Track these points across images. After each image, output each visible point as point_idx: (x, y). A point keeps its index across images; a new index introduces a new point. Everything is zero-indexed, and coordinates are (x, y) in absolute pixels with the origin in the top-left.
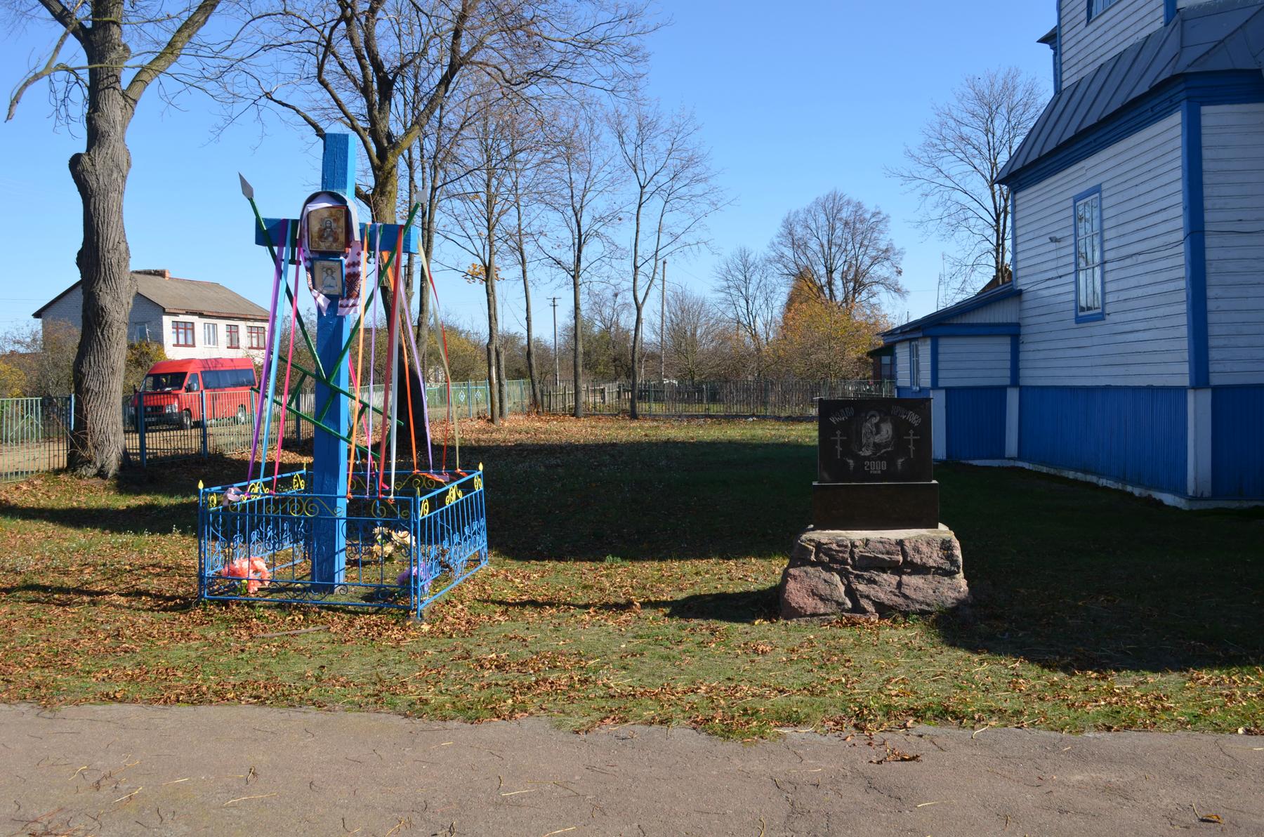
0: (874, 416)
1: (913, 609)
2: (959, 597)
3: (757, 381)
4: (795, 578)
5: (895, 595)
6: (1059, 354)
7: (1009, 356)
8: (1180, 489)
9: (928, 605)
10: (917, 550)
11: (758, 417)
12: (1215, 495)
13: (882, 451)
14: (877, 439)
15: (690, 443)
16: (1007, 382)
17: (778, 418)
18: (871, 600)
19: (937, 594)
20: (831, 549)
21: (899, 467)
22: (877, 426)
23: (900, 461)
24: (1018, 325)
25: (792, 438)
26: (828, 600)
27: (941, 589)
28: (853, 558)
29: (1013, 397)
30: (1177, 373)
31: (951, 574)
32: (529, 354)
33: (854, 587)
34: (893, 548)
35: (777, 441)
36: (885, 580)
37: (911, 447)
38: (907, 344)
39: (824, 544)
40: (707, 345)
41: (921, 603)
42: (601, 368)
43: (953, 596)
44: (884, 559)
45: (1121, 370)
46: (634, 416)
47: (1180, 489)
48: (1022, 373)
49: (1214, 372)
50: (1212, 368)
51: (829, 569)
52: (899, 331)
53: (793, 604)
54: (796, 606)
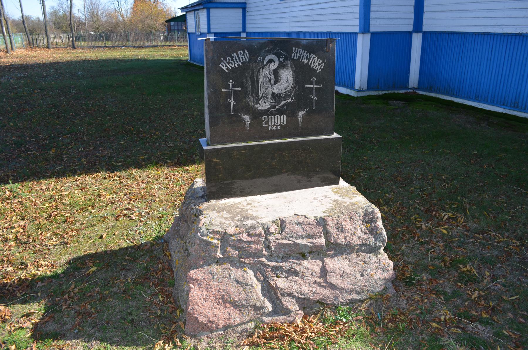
0: (271, 61)
1: (342, 300)
2: (388, 277)
3: (125, 31)
4: (198, 282)
5: (321, 286)
6: (270, 16)
7: (241, 18)
8: (352, 88)
9: (358, 293)
10: (340, 228)
11: (126, 46)
12: (369, 88)
13: (283, 103)
14: (277, 89)
15: (96, 60)
16: (241, 30)
17: (134, 47)
18: (294, 296)
19: (366, 277)
20: (240, 241)
21: (300, 120)
22: (276, 72)
23: (301, 114)
24: (245, 3)
25: (142, 56)
26: (243, 306)
27: (369, 271)
28: (268, 248)
29: (417, 40)
30: (354, 26)
31: (374, 250)
32: (23, 22)
33: (273, 283)
34: (314, 230)
35: (135, 58)
36: (307, 269)
37: (313, 97)
38: (193, 12)
39: (231, 236)
40: (104, 19)
41: (350, 292)
42: (64, 28)
43: (381, 277)
44: (305, 246)
45: (310, 24)
46: (74, 48)
47: (350, 85)
48: (247, 26)
49: (372, 25)
50: (372, 22)
51: (240, 265)
52: (190, 6)
53: (201, 319)
54: (205, 320)
